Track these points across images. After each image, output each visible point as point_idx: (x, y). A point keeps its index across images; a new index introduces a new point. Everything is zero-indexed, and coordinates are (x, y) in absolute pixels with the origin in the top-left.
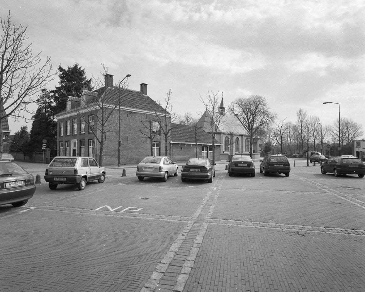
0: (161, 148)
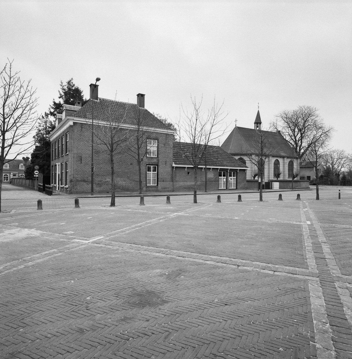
0: (159, 173)
